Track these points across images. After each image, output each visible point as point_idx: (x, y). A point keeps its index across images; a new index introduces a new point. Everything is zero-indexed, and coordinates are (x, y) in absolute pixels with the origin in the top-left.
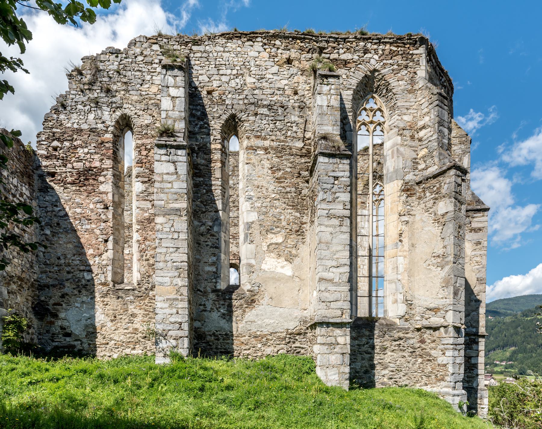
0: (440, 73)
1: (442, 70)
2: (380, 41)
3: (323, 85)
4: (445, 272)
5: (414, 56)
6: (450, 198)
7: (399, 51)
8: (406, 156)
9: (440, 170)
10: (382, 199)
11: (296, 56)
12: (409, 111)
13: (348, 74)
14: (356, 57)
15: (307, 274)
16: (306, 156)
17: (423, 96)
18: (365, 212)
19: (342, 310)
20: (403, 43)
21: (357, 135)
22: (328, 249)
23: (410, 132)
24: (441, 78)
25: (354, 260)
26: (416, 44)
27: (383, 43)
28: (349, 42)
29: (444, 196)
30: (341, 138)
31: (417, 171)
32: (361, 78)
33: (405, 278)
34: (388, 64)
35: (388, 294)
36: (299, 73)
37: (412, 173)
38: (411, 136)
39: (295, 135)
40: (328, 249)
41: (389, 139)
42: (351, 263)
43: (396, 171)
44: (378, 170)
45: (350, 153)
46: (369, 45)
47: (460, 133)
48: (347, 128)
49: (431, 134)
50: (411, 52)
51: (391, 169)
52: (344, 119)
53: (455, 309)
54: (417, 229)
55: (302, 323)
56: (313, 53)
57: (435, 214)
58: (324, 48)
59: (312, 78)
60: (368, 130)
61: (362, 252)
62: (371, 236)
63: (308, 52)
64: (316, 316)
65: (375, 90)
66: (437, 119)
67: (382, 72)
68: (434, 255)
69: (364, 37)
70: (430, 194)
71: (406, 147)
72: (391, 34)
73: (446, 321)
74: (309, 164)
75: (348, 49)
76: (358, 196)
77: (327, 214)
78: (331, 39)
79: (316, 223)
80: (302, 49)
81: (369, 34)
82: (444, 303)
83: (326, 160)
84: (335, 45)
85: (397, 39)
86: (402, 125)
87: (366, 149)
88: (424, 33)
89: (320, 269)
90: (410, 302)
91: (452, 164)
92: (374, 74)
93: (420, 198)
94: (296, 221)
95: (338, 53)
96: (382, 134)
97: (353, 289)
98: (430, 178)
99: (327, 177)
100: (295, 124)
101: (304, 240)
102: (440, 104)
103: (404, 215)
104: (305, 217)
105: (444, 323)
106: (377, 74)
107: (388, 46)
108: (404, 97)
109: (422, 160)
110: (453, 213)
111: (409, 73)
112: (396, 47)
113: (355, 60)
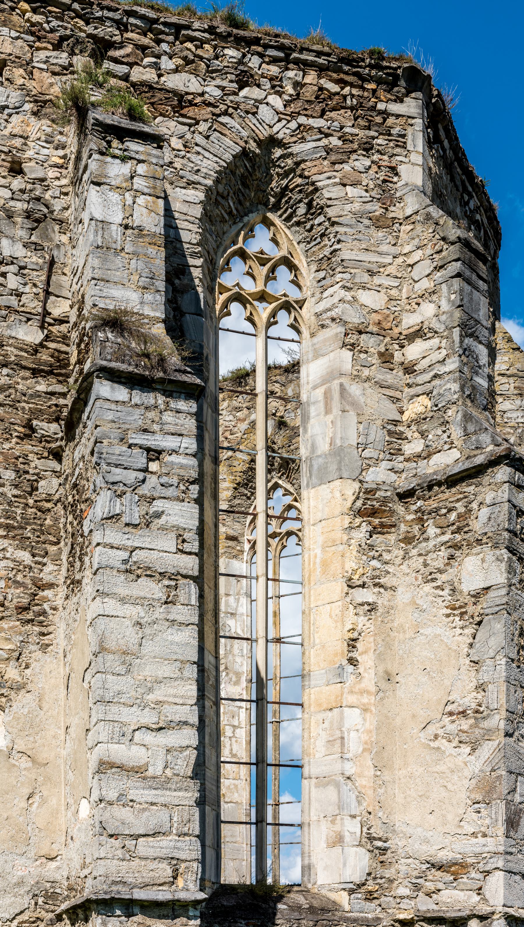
0: (463, 182)
1: (470, 176)
2: (288, 55)
3: (109, 159)
4: (482, 760)
5: (391, 121)
6: (496, 546)
7: (345, 97)
8: (368, 411)
9: (468, 465)
10: (289, 534)
11: (18, 52)
12: (377, 280)
13: (188, 136)
14: (213, 91)
15: (58, 747)
16: (50, 373)
17: (416, 242)
18: (239, 567)
19: (175, 862)
20: (357, 74)
21: (217, 329)
22: (128, 671)
23: (378, 341)
24: (466, 198)
25: (210, 712)
26: (394, 84)
27: (297, 62)
28: (192, 39)
29: (479, 542)
30: (169, 330)
31: (401, 458)
32: (228, 157)
33: (364, 772)
34: (311, 128)
35: (314, 818)
36: (28, 107)
37: (385, 465)
38: (381, 355)
39: (13, 301)
40: (128, 671)
41: (317, 355)
42: (201, 719)
43: (338, 452)
44: (280, 443)
45: (198, 381)
46: (254, 62)
47: (518, 366)
48: (185, 302)
49: (441, 357)
50: (381, 106)
51: (323, 447)
52: (176, 271)
53: (511, 866)
54: (402, 629)
55: (40, 900)
56: (72, 54)
57: (453, 590)
58: (110, 45)
59: (71, 130)
60: (250, 319)
61: (234, 686)
62: (262, 642)
63: (57, 47)
64: (89, 882)
65: (272, 200)
66: (458, 314)
67: (295, 149)
68: (449, 708)
69: (235, 33)
70: (438, 531)
71: (367, 385)
72: (320, 42)
73: (485, 900)
74: (62, 401)
75: (188, 62)
76: (222, 516)
77: (125, 562)
78: (132, 20)
79: (88, 588)
80: (35, 32)
81: (254, 28)
82: (478, 850)
83: (121, 393)
84: (145, 41)
85: (342, 60)
86: (354, 318)
87: (242, 377)
88: (418, 56)
89: (102, 732)
90: (379, 844)
91: (500, 450)
92: (271, 153)
93: (408, 540)
94: (19, 578)
95: (156, 66)
96: (296, 337)
97: (208, 801)
98: (439, 484)
99: (124, 448)
100: (13, 268)
101: (46, 640)
102: (468, 273)
103: (363, 586)
104: (50, 567)
105: (481, 906)
106: (278, 152)
107: (311, 77)
108: (360, 236)
109: (414, 428)
110: (504, 591)
111: (375, 168)
112: (337, 82)
113: (212, 100)
